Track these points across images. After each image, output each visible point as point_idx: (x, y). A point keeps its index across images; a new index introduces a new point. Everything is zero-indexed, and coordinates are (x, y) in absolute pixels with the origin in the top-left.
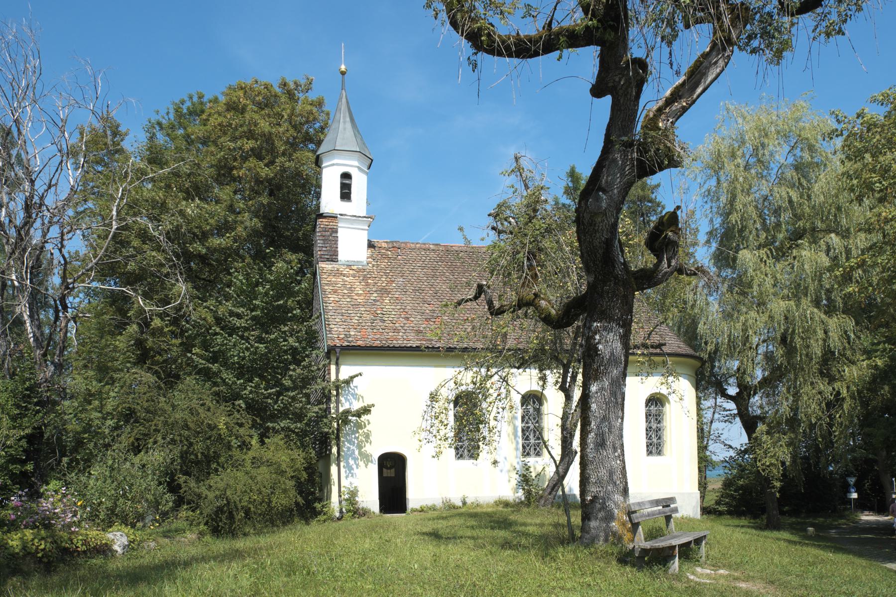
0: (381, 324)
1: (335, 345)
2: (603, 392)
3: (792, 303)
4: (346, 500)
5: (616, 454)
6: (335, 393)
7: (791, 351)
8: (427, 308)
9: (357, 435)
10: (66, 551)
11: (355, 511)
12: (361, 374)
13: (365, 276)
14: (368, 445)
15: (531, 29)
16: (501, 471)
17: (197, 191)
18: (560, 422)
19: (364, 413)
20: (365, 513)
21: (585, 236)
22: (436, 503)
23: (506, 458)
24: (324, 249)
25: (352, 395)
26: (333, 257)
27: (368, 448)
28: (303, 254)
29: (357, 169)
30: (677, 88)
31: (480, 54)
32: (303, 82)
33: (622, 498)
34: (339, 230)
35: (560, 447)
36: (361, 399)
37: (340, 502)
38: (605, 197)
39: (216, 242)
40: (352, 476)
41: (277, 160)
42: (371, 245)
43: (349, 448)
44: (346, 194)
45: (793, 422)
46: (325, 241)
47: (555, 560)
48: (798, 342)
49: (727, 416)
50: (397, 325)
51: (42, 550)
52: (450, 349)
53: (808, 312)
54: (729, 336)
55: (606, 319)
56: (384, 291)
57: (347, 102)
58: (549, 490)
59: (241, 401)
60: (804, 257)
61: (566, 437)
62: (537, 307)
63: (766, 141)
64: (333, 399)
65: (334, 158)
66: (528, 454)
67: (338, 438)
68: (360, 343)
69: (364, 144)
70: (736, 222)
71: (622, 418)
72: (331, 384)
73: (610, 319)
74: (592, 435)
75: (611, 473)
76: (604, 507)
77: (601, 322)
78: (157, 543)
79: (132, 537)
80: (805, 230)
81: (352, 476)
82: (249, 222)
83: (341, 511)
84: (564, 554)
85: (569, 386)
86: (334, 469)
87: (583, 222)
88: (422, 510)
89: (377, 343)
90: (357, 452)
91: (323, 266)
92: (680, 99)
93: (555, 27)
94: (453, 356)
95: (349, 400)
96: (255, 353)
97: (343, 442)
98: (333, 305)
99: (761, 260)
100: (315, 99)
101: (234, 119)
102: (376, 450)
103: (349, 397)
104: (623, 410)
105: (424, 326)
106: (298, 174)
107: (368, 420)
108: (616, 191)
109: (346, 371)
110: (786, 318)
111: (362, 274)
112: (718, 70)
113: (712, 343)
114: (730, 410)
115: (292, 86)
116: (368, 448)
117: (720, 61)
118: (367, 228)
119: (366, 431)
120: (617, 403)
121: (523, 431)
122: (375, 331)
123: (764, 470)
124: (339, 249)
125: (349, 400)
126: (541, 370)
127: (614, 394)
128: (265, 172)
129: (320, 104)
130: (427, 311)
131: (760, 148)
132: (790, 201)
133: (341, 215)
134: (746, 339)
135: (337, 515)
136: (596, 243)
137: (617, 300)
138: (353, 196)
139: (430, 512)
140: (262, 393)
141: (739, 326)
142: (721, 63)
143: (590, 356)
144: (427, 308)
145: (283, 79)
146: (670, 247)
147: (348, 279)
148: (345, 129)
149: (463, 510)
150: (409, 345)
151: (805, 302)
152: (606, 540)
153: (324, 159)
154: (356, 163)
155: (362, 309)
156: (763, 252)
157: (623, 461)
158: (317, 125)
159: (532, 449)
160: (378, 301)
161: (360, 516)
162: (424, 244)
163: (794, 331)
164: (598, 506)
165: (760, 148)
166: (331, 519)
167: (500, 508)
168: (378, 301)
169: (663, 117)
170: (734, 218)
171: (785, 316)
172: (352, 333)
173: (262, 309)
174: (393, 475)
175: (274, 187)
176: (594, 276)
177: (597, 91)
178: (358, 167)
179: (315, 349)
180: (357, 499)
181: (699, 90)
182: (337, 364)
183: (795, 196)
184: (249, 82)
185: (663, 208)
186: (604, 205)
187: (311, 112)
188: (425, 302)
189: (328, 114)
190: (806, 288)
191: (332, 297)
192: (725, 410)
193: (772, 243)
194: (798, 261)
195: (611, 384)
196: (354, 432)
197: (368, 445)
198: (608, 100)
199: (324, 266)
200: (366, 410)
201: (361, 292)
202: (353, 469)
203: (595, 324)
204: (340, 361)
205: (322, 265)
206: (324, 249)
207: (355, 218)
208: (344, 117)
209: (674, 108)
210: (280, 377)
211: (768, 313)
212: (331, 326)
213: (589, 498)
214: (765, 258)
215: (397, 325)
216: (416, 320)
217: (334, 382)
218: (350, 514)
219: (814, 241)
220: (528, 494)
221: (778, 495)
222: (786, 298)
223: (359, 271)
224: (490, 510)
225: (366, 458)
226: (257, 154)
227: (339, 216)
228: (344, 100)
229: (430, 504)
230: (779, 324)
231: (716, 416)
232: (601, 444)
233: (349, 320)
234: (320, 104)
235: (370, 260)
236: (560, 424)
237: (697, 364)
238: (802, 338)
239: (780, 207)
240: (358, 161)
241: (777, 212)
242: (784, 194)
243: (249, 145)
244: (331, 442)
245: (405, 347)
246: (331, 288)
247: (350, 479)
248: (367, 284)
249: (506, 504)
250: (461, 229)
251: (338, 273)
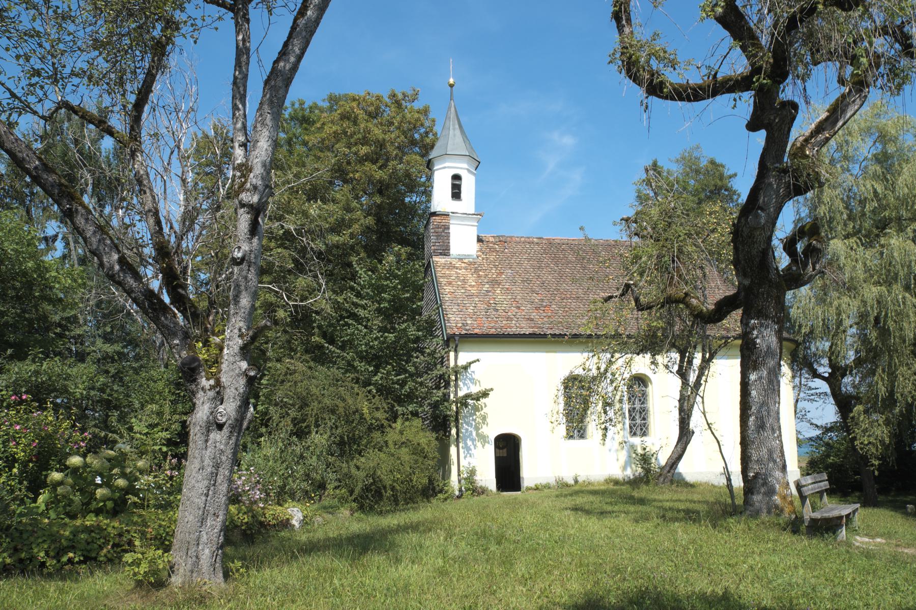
0: (494, 313)
2: (763, 380)
3: (883, 288)
4: (465, 479)
5: (776, 435)
6: (453, 378)
7: (884, 333)
8: (536, 298)
9: (474, 417)
10: (261, 524)
11: (473, 489)
12: (478, 360)
13: (476, 269)
14: (485, 426)
15: (695, 78)
16: (610, 450)
17: (314, 194)
18: (677, 404)
19: (482, 397)
20: (483, 491)
21: (743, 246)
22: (550, 482)
24: (437, 244)
25: (470, 379)
26: (445, 252)
27: (484, 430)
28: (410, 248)
30: (821, 122)
31: (650, 97)
32: (409, 92)
33: (781, 474)
34: (451, 226)
35: (678, 427)
36: (478, 383)
37: (460, 481)
38: (763, 215)
39: (334, 239)
40: (470, 456)
41: (390, 164)
42: (480, 240)
43: (467, 430)
44: (456, 194)
45: (890, 400)
46: (438, 236)
47: (729, 532)
48: (891, 325)
49: (812, 395)
50: (509, 314)
51: (247, 523)
52: (576, 336)
53: (900, 297)
54: (823, 320)
55: (763, 317)
56: (495, 283)
57: (456, 111)
58: (668, 468)
59: (372, 387)
60: (893, 246)
61: (684, 418)
62: (688, 305)
63: (850, 138)
64: (452, 384)
66: (635, 434)
67: (457, 420)
68: (476, 331)
69: (472, 148)
70: (825, 214)
71: (779, 403)
72: (450, 369)
73: (767, 317)
74: (752, 419)
75: (770, 452)
76: (765, 484)
77: (758, 319)
78: (323, 518)
79: (306, 512)
80: (891, 220)
81: (470, 456)
82: (363, 221)
83: (460, 490)
84: (736, 525)
85: (686, 370)
86: (453, 450)
87: (741, 235)
88: (537, 488)
89: (493, 331)
90: (474, 433)
91: (437, 259)
92: (824, 131)
93: (720, 76)
94: (577, 344)
95: (466, 385)
96: (384, 343)
97: (462, 424)
98: (449, 296)
99: (852, 249)
100: (421, 108)
101: (349, 128)
102: (493, 431)
103: (468, 381)
104: (779, 396)
105: (534, 314)
106: (408, 175)
108: (772, 210)
109: (464, 357)
110: (879, 302)
111: (473, 266)
112: (856, 107)
113: (806, 326)
114: (816, 389)
115: (400, 96)
116: (484, 430)
117: (858, 100)
118: (476, 224)
119: (483, 413)
120: (774, 390)
121: (629, 411)
122: (489, 319)
123: (862, 449)
124: (451, 244)
125: (466, 385)
126: (653, 356)
127: (770, 382)
128: (379, 175)
129: (425, 112)
130: (536, 300)
131: (844, 145)
132: (875, 192)
134: (840, 323)
135: (457, 493)
136: (754, 252)
137: (772, 300)
138: (462, 195)
139: (546, 491)
140: (392, 379)
141: (833, 311)
142: (858, 102)
143: (748, 349)
144: (536, 298)
145: (393, 91)
146: (815, 254)
147: (460, 272)
148: (455, 135)
149: (577, 488)
150: (522, 333)
151: (897, 288)
152: (769, 512)
153: (435, 163)
154: (465, 166)
155: (477, 299)
156: (852, 240)
157: (781, 441)
158: (422, 130)
159: (639, 429)
160: (490, 291)
161: (479, 494)
162: (528, 238)
163: (886, 315)
164: (760, 481)
165: (844, 145)
166: (451, 496)
167: (611, 486)
168: (490, 291)
169: (809, 145)
170: (822, 210)
171: (877, 300)
172: (469, 322)
173: (389, 302)
174: (505, 455)
175: (382, 188)
176: (750, 280)
177: (752, 126)
178: (468, 169)
179: (435, 337)
180: (475, 478)
181: (840, 123)
182: (456, 351)
183: (879, 189)
184: (362, 94)
185: (739, 195)
186: (763, 221)
187: (418, 120)
188: (533, 291)
189: (434, 121)
190: (896, 274)
191: (448, 289)
192: (810, 389)
193: (859, 231)
194: (887, 249)
195: (769, 373)
196: (472, 415)
197: (485, 426)
198: (762, 134)
199: (438, 260)
200: (485, 394)
201: (473, 283)
202: (471, 450)
203: (752, 321)
204: (458, 349)
205: (435, 259)
206: (437, 244)
208: (454, 125)
209: (818, 139)
210: (404, 363)
211: (860, 298)
212: (449, 316)
213: (751, 474)
214: (855, 247)
215: (509, 314)
216: (527, 308)
217: (452, 368)
218: (470, 492)
219: (901, 230)
220: (647, 471)
221: (876, 473)
222: (877, 283)
223: (470, 264)
224: (602, 488)
225: (483, 439)
226: (372, 159)
228: (453, 109)
229: (544, 482)
230: (872, 307)
231: (802, 395)
232: (761, 426)
233: (464, 310)
234: (425, 112)
235: (479, 253)
236: (678, 406)
237: (793, 346)
238: (895, 321)
239: (866, 199)
240: (468, 164)
241: (863, 202)
242: (869, 186)
243: (364, 150)
244: (450, 424)
245: (519, 334)
246: (446, 280)
247: (468, 459)
248: (479, 276)
249: (616, 482)
250: (582, 229)
251: (451, 266)
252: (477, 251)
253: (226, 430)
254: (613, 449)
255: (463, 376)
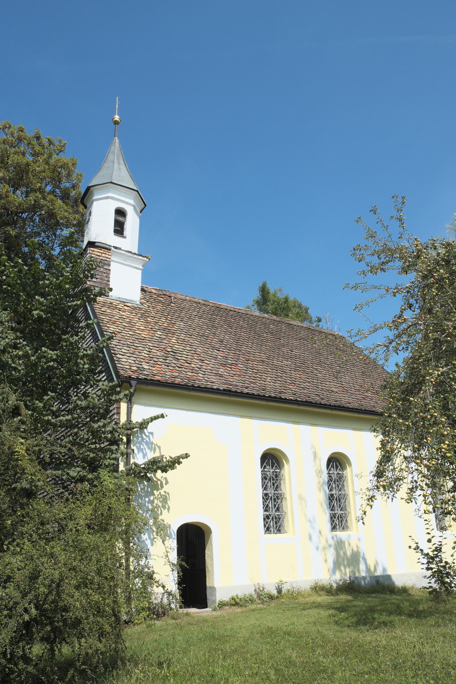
1: (130, 377)
9: (152, 498)
14: (165, 512)
16: (317, 548)
23: (320, 532)
25: (147, 443)
29: (132, 207)
34: (112, 263)
42: (143, 290)
65: (109, 192)
68: (157, 378)
107: (166, 479)
119: (163, 493)
133: (116, 248)
147: (124, 314)
153: (95, 194)
154: (132, 202)
161: (158, 616)
182: (130, 402)
197: (165, 512)
204: (133, 399)
207: (130, 254)
208: (118, 160)
212: (118, 356)
215: (193, 365)
227: (113, 248)
249: (328, 591)
251: (111, 305)
252: (141, 299)
253: (148, 539)
254: (321, 547)
255: (138, 437)
